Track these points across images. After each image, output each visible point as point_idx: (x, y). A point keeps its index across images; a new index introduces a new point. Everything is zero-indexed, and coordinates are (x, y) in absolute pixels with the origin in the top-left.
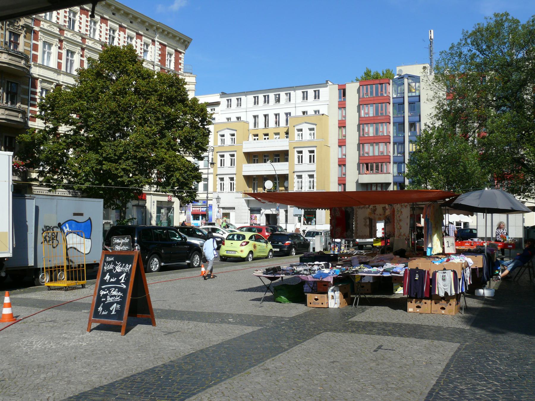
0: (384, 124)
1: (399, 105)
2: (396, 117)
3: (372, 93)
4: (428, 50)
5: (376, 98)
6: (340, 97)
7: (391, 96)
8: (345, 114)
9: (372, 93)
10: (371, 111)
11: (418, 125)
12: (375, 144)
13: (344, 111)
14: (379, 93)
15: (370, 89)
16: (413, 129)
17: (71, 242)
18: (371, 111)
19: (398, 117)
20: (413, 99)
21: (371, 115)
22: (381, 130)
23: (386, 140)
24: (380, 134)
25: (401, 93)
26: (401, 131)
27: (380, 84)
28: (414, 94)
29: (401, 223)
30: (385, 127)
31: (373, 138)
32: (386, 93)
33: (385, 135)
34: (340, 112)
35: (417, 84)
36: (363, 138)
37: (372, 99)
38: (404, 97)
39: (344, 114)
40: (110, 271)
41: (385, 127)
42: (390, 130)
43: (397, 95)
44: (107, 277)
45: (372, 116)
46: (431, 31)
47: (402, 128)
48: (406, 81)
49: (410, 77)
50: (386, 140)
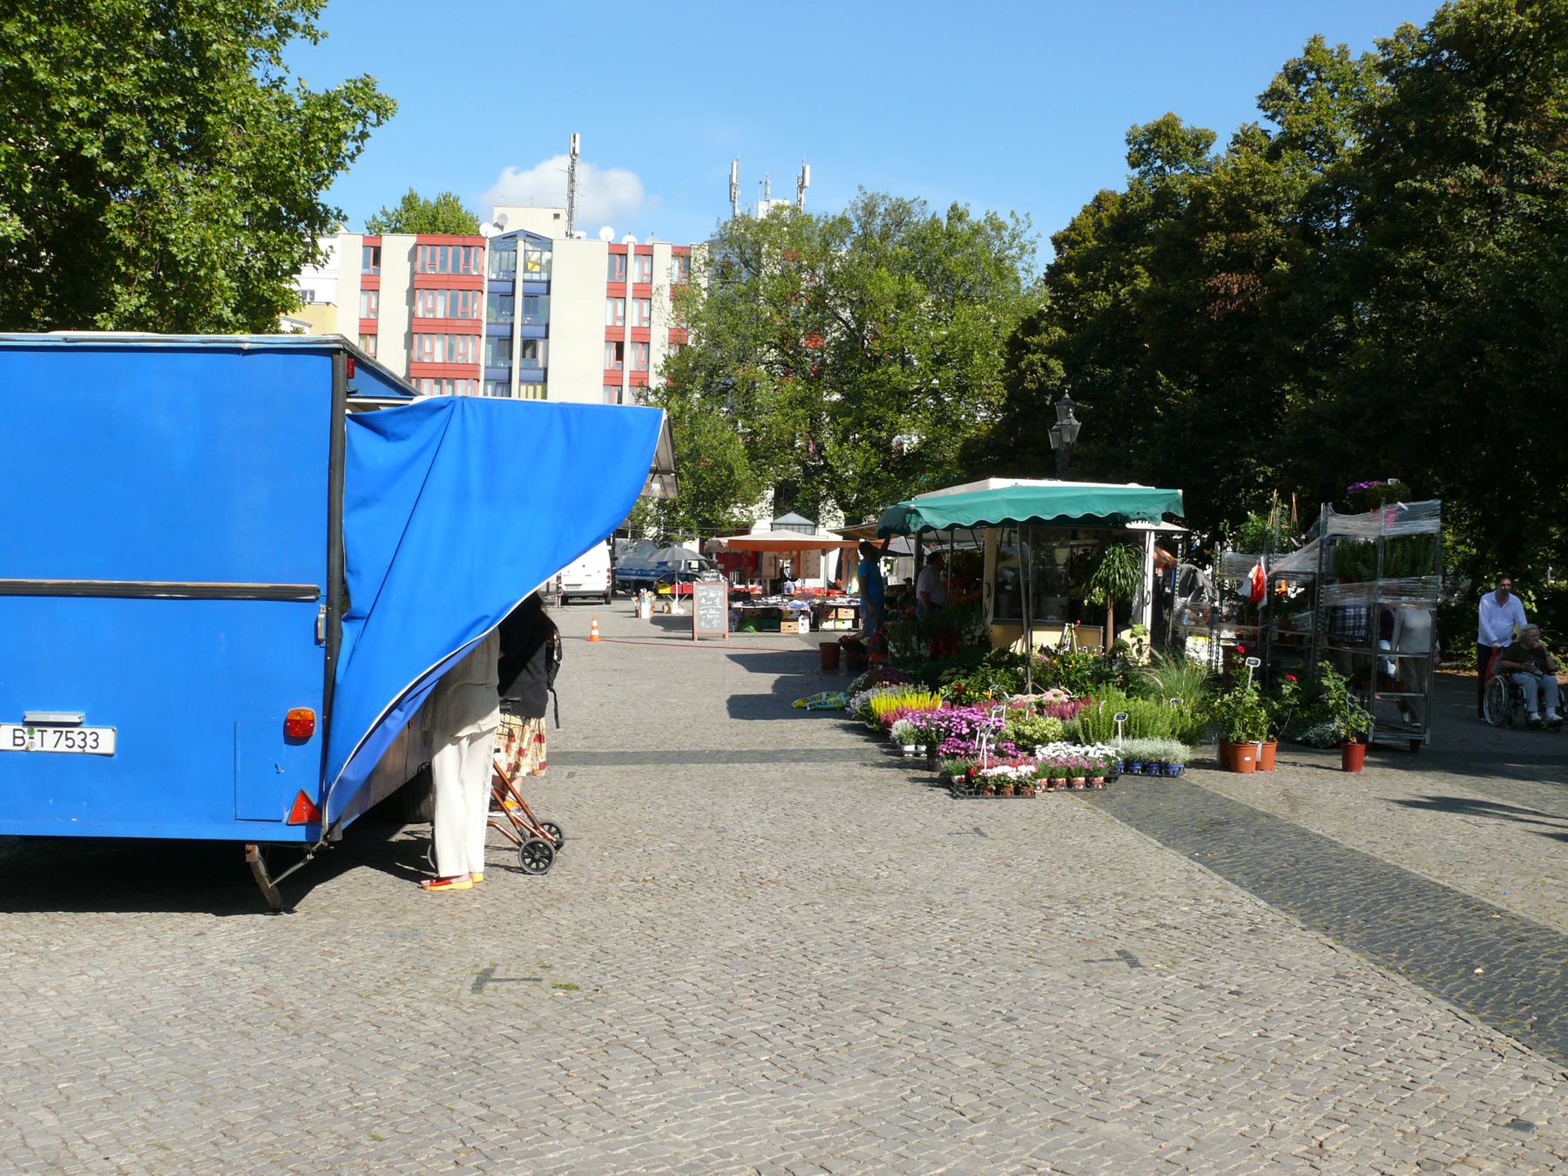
0: (469, 337)
1: (503, 298)
2: (494, 324)
3: (444, 264)
4: (566, 176)
5: (452, 278)
6: (365, 265)
7: (486, 275)
8: (378, 304)
9: (444, 264)
10: (436, 306)
11: (541, 345)
12: (444, 381)
13: (374, 299)
14: (461, 267)
15: (441, 255)
16: (529, 352)
17: (909, 562)
18: (436, 306)
19: (498, 324)
20: (533, 288)
21: (440, 315)
22: (461, 351)
23: (469, 372)
24: (460, 360)
25: (507, 272)
26: (504, 356)
27: (464, 246)
28: (536, 277)
29: (808, 564)
30: (470, 344)
31: (442, 367)
32: (476, 268)
33: (470, 362)
34: (365, 298)
35: (547, 255)
36: (417, 366)
37: (446, 278)
38: (514, 282)
39: (373, 306)
40: (705, 597)
41: (470, 344)
42: (478, 352)
43: (499, 275)
44: (703, 601)
45: (442, 316)
46: (574, 137)
47: (507, 349)
48: (521, 244)
49: (530, 236)
50: (469, 372)
